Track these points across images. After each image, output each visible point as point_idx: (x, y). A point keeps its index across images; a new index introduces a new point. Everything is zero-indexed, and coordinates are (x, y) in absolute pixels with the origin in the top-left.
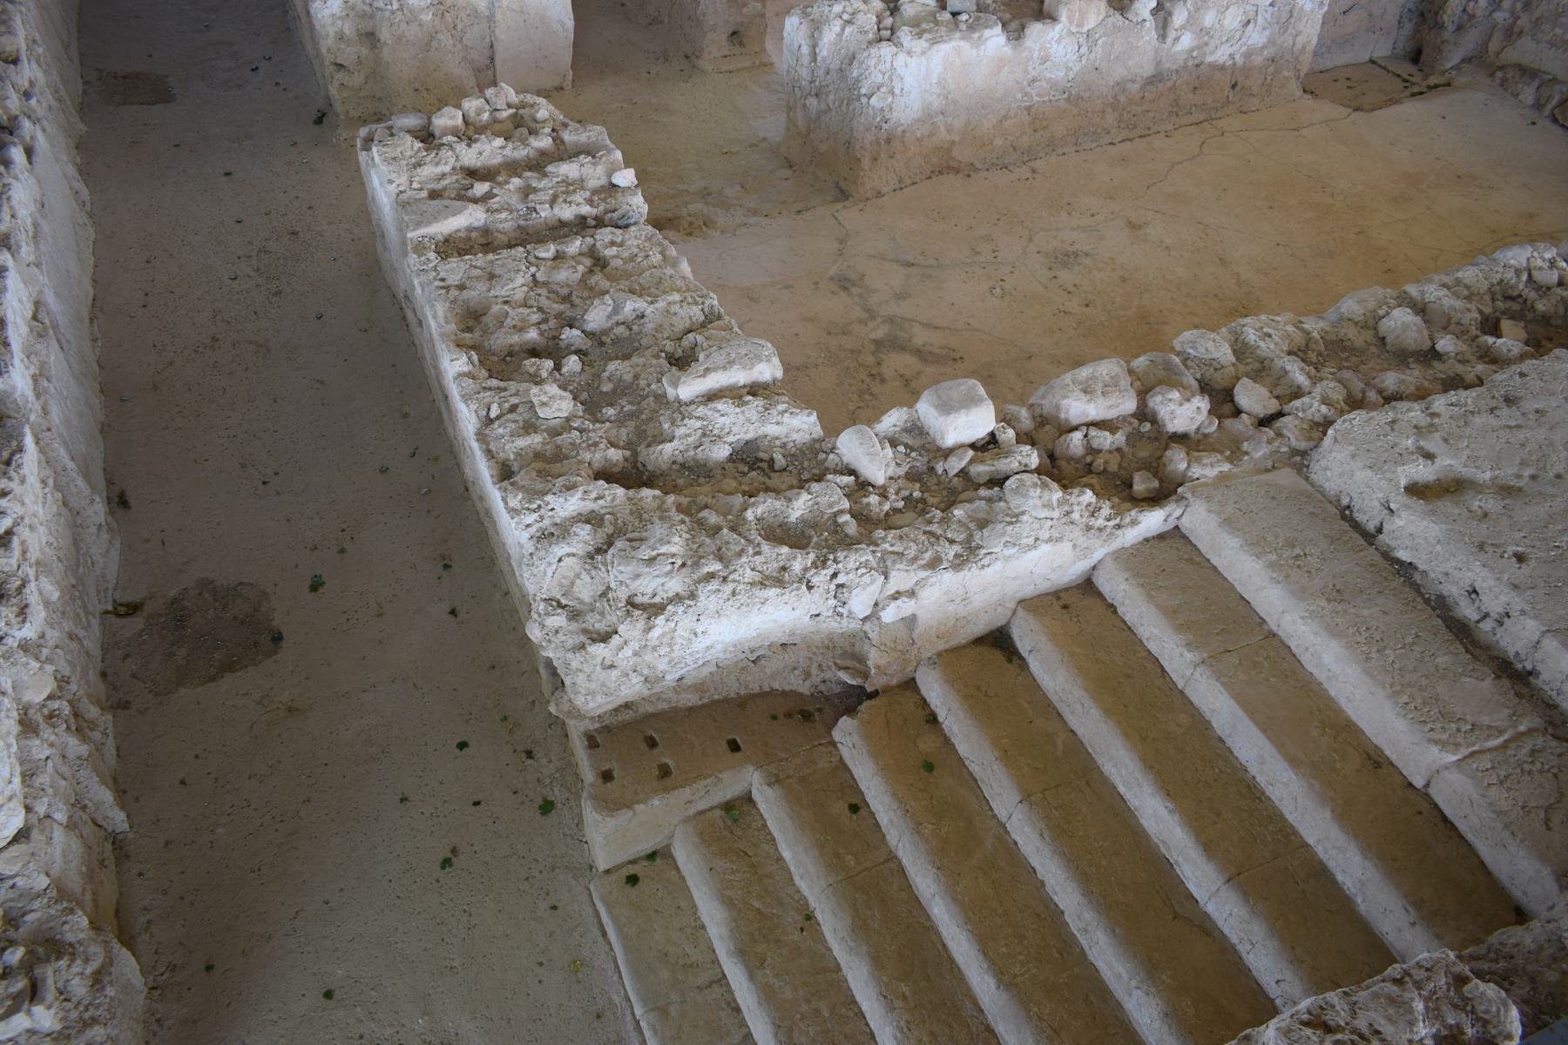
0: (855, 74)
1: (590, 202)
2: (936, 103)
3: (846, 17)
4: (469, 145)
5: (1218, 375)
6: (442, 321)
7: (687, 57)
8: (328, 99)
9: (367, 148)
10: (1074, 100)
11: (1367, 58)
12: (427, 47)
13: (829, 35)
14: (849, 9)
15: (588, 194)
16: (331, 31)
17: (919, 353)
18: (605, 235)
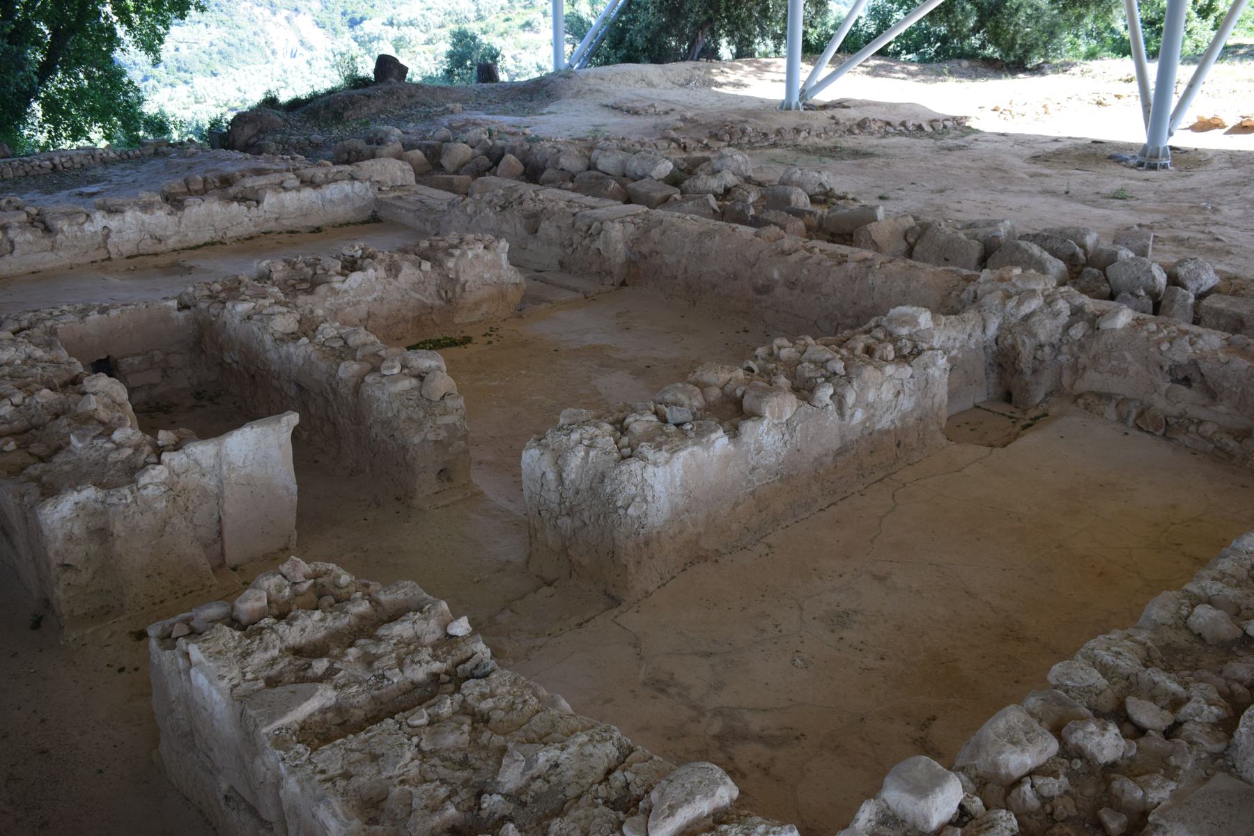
0: (608, 490)
1: (435, 657)
2: (681, 502)
3: (586, 442)
5: (1101, 699)
6: (342, 817)
8: (47, 603)
11: (971, 405)
13: (575, 461)
15: (430, 650)
17: (760, 738)
18: (472, 689)
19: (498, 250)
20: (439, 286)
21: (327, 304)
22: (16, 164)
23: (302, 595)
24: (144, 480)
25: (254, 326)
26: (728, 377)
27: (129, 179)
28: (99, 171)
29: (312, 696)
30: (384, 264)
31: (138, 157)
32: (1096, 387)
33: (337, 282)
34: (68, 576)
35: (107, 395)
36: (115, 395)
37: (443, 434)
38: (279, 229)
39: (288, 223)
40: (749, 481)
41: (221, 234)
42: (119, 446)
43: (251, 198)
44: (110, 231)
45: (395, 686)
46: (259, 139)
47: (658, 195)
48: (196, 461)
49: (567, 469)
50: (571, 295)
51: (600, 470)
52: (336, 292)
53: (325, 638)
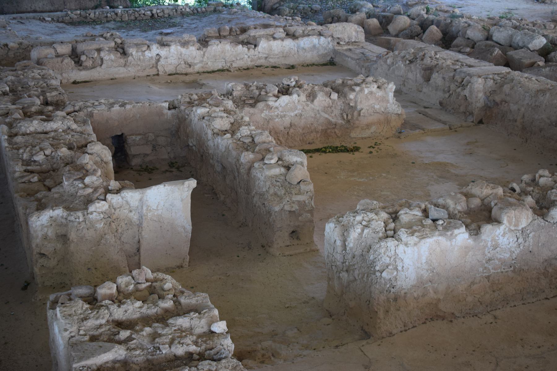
0: (372, 257)
1: (196, 343)
2: (426, 275)
3: (364, 223)
4: (119, 306)
7: (263, 246)
9: (53, 308)
10: (518, 271)
12: (99, 243)
13: (354, 234)
14: (366, 219)
15: (195, 337)
16: (40, 234)
19: (388, 90)
20: (343, 111)
21: (263, 115)
22: (131, 12)
23: (140, 291)
24: (91, 208)
25: (204, 123)
26: (490, 192)
27: (194, 26)
28: (178, 20)
29: (109, 351)
30: (306, 92)
31: (203, 13)
33: (271, 102)
34: (42, 261)
35: (98, 155)
36: (103, 156)
37: (295, 207)
38: (266, 65)
39: (273, 61)
40: (485, 268)
41: (229, 65)
42: (86, 186)
43: (252, 43)
45: (163, 355)
46: (280, 5)
47: (527, 61)
48: (127, 202)
49: (349, 239)
50: (439, 126)
51: (369, 243)
52: (270, 108)
53: (138, 319)
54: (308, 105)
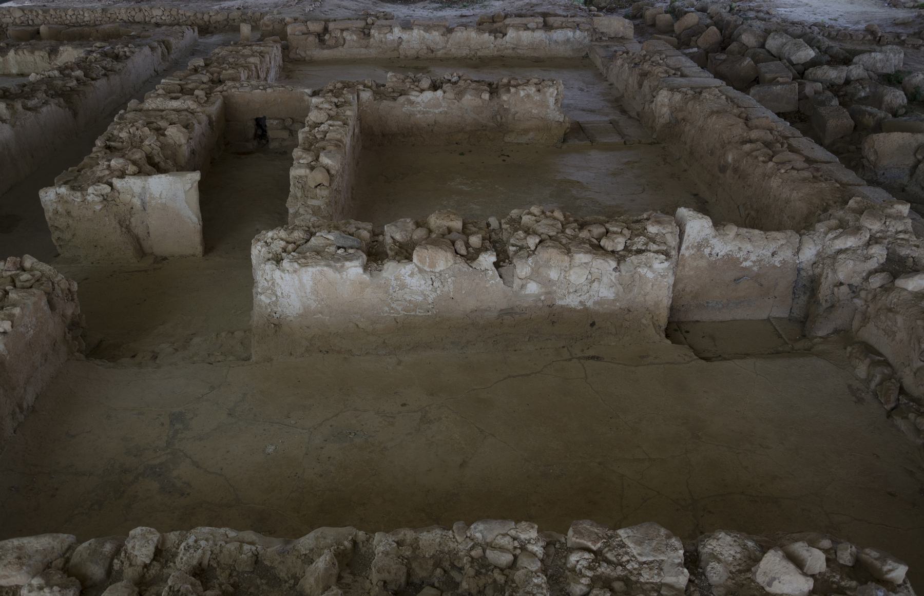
11: (765, 316)
32: (873, 341)
44: (402, 41)
52: (412, 103)
54: (454, 103)
